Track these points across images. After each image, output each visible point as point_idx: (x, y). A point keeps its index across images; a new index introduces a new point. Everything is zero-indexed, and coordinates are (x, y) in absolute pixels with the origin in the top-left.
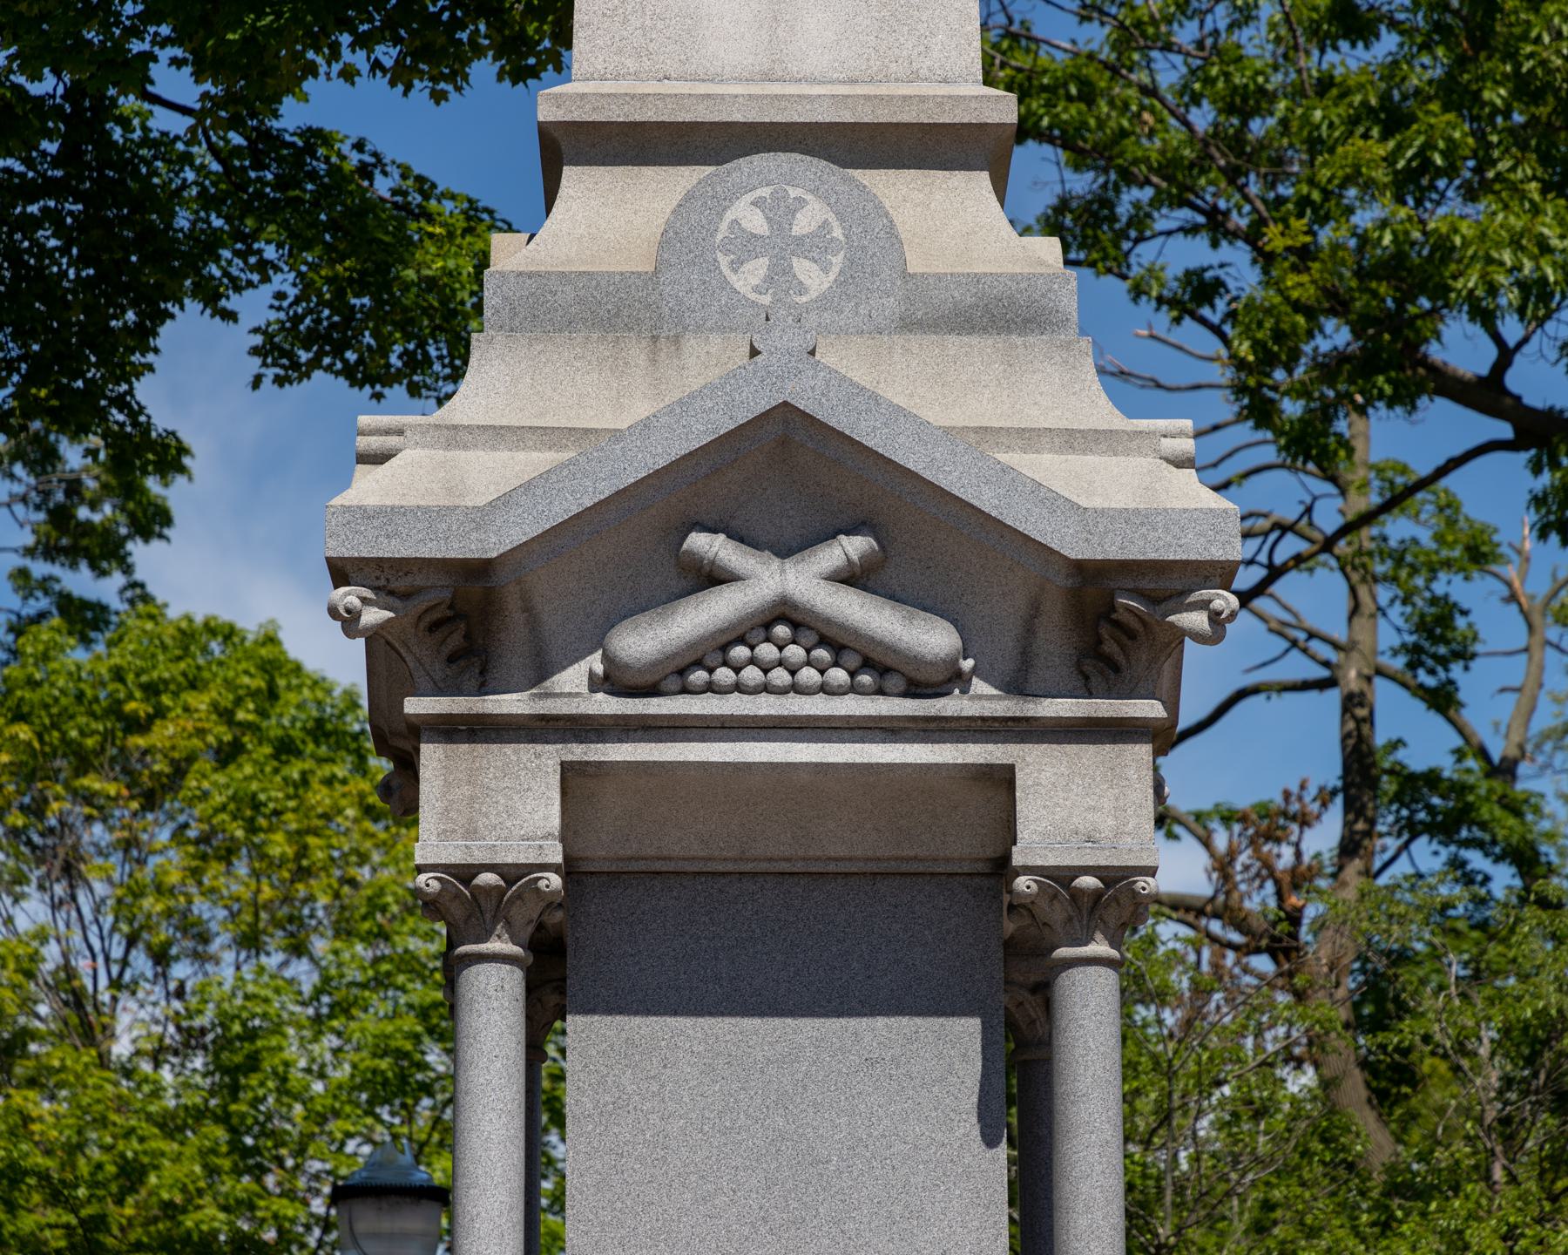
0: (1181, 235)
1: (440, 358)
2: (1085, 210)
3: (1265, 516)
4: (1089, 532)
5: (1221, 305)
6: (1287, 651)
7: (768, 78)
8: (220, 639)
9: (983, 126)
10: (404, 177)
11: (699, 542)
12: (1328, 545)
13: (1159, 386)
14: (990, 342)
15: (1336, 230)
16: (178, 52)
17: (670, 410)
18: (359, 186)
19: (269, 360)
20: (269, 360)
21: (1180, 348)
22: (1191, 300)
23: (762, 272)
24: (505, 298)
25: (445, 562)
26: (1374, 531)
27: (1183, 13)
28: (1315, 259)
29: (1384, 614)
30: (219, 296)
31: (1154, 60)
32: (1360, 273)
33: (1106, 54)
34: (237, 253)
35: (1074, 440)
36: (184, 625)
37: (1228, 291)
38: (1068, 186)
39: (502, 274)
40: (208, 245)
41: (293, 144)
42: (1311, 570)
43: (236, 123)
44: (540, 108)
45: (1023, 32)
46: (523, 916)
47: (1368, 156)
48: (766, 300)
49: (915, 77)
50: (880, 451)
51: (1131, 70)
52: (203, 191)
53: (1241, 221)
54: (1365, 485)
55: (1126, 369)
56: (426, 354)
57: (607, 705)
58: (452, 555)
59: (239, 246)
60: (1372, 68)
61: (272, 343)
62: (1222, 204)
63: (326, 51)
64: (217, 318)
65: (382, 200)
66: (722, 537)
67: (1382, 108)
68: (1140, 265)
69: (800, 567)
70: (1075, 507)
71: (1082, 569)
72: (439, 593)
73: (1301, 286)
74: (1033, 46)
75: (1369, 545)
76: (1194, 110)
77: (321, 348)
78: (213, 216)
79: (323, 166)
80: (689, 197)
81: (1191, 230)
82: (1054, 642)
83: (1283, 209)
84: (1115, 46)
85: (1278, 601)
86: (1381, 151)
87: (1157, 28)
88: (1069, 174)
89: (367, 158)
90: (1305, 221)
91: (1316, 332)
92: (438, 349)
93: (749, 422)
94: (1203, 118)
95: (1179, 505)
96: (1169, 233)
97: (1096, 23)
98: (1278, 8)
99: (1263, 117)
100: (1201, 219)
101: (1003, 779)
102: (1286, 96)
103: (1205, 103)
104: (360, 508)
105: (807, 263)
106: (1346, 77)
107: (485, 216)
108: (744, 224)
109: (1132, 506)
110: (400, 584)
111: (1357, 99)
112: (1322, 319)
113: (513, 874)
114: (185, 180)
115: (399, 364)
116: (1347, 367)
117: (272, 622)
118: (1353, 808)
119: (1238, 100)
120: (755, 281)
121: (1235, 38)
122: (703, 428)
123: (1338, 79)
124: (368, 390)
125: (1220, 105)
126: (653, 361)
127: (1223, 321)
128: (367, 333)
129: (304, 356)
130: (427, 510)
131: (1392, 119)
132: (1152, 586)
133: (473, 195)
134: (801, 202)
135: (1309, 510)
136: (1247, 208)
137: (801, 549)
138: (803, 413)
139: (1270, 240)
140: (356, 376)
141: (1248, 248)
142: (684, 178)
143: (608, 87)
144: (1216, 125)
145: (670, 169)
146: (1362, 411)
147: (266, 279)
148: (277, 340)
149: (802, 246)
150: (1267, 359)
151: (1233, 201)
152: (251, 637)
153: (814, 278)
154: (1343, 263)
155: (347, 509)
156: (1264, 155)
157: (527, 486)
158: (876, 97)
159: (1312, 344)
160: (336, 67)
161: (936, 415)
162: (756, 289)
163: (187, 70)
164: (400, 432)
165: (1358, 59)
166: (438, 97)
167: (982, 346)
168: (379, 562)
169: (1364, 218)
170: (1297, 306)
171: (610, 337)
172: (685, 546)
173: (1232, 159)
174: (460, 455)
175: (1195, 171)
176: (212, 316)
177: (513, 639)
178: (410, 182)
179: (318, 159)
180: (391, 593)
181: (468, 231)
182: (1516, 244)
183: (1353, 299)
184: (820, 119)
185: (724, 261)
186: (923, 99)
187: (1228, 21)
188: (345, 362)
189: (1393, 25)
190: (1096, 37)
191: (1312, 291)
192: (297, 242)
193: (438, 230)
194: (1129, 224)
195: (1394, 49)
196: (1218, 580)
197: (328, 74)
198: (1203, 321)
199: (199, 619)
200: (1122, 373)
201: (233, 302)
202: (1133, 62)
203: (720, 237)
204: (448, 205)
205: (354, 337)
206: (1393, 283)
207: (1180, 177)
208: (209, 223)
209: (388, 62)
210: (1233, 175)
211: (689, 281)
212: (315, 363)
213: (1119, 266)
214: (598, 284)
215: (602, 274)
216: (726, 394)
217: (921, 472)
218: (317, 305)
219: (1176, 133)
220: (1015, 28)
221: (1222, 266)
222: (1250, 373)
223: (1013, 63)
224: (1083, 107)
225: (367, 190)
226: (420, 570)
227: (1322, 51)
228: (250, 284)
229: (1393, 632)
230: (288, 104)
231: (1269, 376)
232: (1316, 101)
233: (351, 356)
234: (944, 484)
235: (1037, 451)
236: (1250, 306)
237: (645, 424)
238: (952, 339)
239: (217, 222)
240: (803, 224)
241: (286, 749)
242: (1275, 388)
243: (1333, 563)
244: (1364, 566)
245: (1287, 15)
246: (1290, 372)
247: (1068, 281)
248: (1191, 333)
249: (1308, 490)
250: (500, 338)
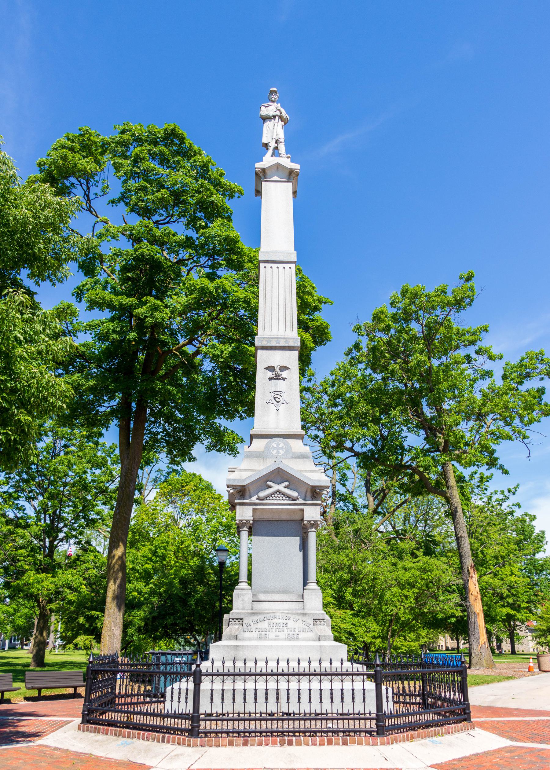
11: (269, 483)
35: (311, 471)
46: (248, 525)
53: (321, 428)
57: (258, 501)
71: (312, 486)
72: (239, 489)
82: (309, 495)
101: (303, 510)
113: (247, 521)
118: (333, 498)
131: (340, 418)
140: (217, 450)
153: (282, 452)
161: (296, 468)
167: (301, 460)
177: (247, 494)
182: (356, 433)
240: (281, 446)
241: (203, 489)
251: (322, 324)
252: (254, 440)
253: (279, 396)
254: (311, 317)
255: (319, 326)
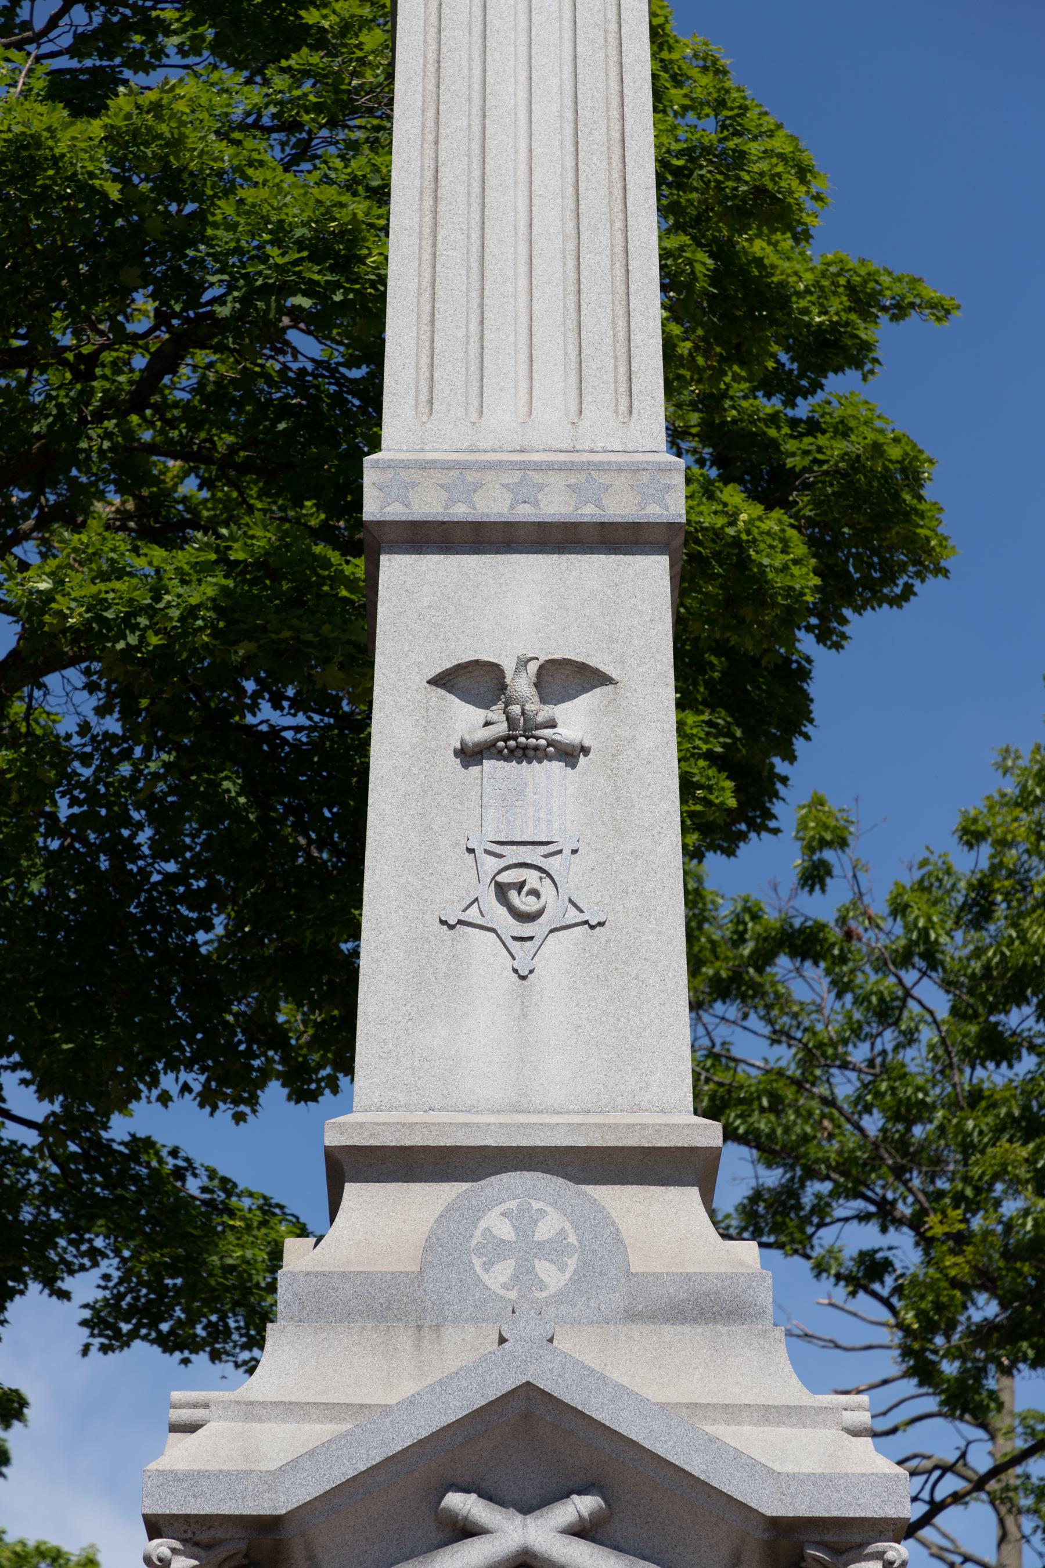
0: (855, 1222)
1: (238, 1328)
2: (775, 1201)
3: (929, 1458)
4: (782, 1493)
5: (889, 1281)
6: (920, 979)
7: (515, 1109)
8: (48, 1561)
9: (693, 1150)
10: (211, 1178)
11: (456, 1501)
12: (979, 1484)
13: (837, 1346)
14: (699, 1331)
15: (985, 1219)
16: (27, 1075)
17: (431, 1389)
18: (175, 1187)
19: (96, 1332)
20: (96, 1332)
21: (855, 1315)
22: (864, 1276)
23: (510, 1272)
24: (295, 1294)
25: (241, 1517)
26: (1019, 1470)
27: (858, 1036)
28: (968, 1244)
29: (1028, 1541)
30: (55, 1279)
31: (832, 1075)
32: (1006, 1255)
33: (794, 1071)
34: (71, 1242)
36: (18, 1549)
37: (895, 1270)
38: (761, 1181)
39: (294, 1274)
40: (47, 1234)
41: (120, 1153)
42: (966, 1503)
43: (74, 1136)
44: (326, 1134)
45: (724, 1052)
47: (1013, 1157)
48: (513, 1295)
49: (637, 1109)
50: (607, 1423)
51: (813, 1084)
52: (44, 1191)
53: (905, 1210)
54: (1011, 1430)
55: (810, 1332)
56: (226, 1325)
58: (248, 1512)
59: (73, 1236)
60: (1014, 1084)
61: (99, 1317)
62: (890, 1196)
63: (147, 1078)
64: (54, 1298)
65: (194, 1198)
66: (474, 1496)
67: (1022, 1117)
68: (821, 1246)
69: (539, 1522)
70: (771, 1471)
71: (775, 1523)
73: (957, 1265)
74: (732, 1064)
75: (1014, 1482)
76: (866, 1117)
77: (139, 1320)
78: (52, 1211)
79: (145, 1171)
80: (449, 1209)
81: (863, 1218)
83: (942, 1202)
84: (802, 1063)
85: (938, 1529)
86: (1024, 1153)
87: (836, 1049)
88: (762, 1171)
89: (181, 1163)
90: (959, 1212)
91: (969, 1304)
92: (236, 1321)
93: (497, 1399)
94: (873, 1124)
95: (858, 1470)
96: (846, 1220)
97: (784, 1046)
98: (936, 1032)
99: (924, 1124)
100: (872, 1209)
102: (943, 1107)
103: (875, 1111)
104: (171, 1472)
105: (547, 1264)
106: (993, 1091)
107: (277, 1211)
108: (495, 1231)
109: (819, 1471)
110: (204, 1537)
111: (1003, 1111)
112: (975, 1294)
114: (29, 1180)
115: (203, 1334)
116: (996, 1335)
117: (92, 1546)
119: (903, 1110)
120: (503, 1279)
121: (900, 1056)
122: (458, 1404)
123: (986, 1093)
124: (178, 1355)
125: (889, 1114)
126: (418, 1347)
127: (892, 1294)
128: (177, 1308)
129: (125, 1327)
130: (227, 1474)
132: (835, 1539)
133: (268, 1194)
134: (542, 1213)
135: (963, 1456)
136: (910, 1199)
137: (540, 1507)
138: (543, 1391)
139: (931, 1228)
140: (168, 1343)
141: (912, 1233)
142: (446, 1192)
143: (383, 1117)
144: (884, 1130)
145: (434, 1185)
146: (1007, 1372)
147: (95, 1264)
148: (102, 1314)
149: (542, 1249)
150: (929, 1328)
151: (899, 1192)
152: (74, 1559)
154: (992, 1246)
155: (160, 1473)
156: (924, 1155)
157: (312, 1454)
158: (604, 1125)
159: (966, 1315)
160: (155, 1092)
161: (654, 1393)
162: (504, 1286)
163: (33, 1088)
164: (206, 1406)
165: (1003, 1076)
166: (239, 1118)
168: (187, 1518)
169: (1010, 1207)
170: (954, 1283)
171: (382, 1326)
172: (443, 1504)
173: (899, 1160)
174: (257, 1426)
175: (868, 1168)
176: (50, 1295)
178: (216, 1182)
179: (140, 1164)
180: (197, 1544)
181: (264, 1223)
183: (1001, 1277)
184: (559, 1143)
185: (477, 1262)
186: (644, 1127)
187: (894, 1043)
188: (159, 1332)
189: (1032, 1048)
190: (785, 1056)
191: (967, 1270)
192: (120, 1232)
193: (238, 1223)
194: (812, 1212)
195: (1033, 1068)
196: (891, 1534)
197: (148, 1098)
198: (874, 1295)
199: (31, 1543)
200: (806, 1335)
201: (68, 1283)
202: (816, 1078)
203: (474, 1242)
204: (247, 1202)
205: (167, 1312)
206: (1034, 1263)
207: (854, 1172)
208: (48, 1215)
209: (197, 1087)
210: (899, 1172)
211: (448, 1279)
212: (133, 1335)
213: (804, 1248)
214: (373, 1282)
215: (377, 1274)
216: (479, 1375)
217: (642, 1442)
218: (137, 1284)
219: (852, 1140)
220: (717, 1049)
221: (890, 1248)
222: (915, 1339)
223: (716, 1078)
224: (772, 1118)
225: (180, 1190)
226: (221, 1525)
227: (973, 1068)
228: (83, 1268)
229: (1036, 1557)
230: (116, 1120)
231: (930, 1341)
232: (967, 1112)
233: (165, 1327)
234: (661, 1452)
235: (739, 1424)
236: (914, 1281)
237: (411, 1401)
238: (668, 1328)
239: (55, 1215)
240: (544, 1231)
242: (935, 1352)
243: (984, 1496)
244: (1010, 1499)
245: (943, 1041)
246: (948, 1337)
247: (764, 1280)
248: (863, 1302)
249: (963, 1437)
250: (291, 1327)
251: (877, 449)
252: (351, 1190)
253: (532, 878)
254: (803, 409)
255: (855, 462)
